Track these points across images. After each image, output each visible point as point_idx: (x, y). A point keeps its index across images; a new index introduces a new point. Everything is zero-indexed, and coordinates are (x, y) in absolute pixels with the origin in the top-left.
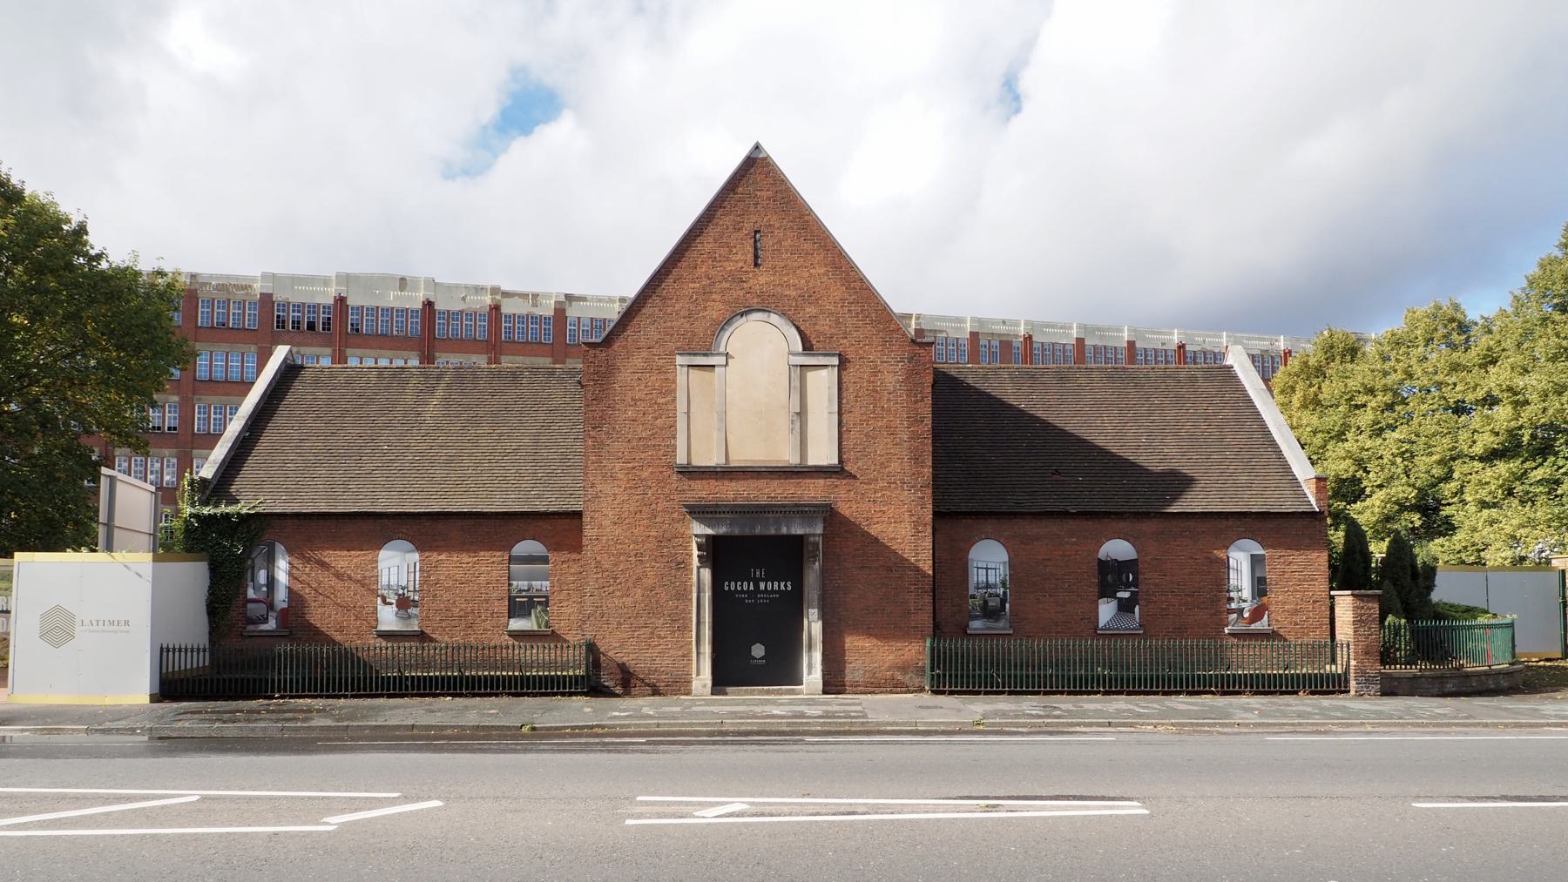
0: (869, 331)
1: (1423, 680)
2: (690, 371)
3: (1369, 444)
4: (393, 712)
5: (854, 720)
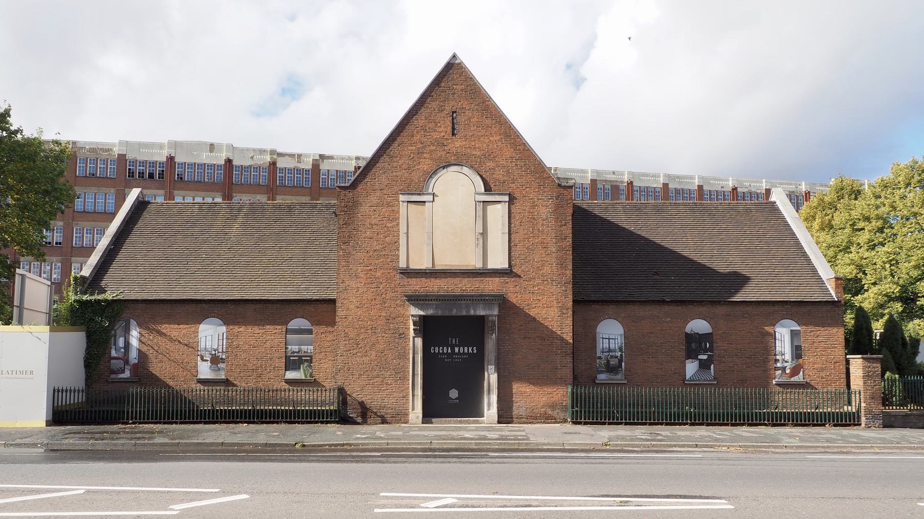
0: (529, 178)
1: (912, 417)
2: (409, 205)
3: (866, 255)
4: (208, 433)
5: (520, 442)
